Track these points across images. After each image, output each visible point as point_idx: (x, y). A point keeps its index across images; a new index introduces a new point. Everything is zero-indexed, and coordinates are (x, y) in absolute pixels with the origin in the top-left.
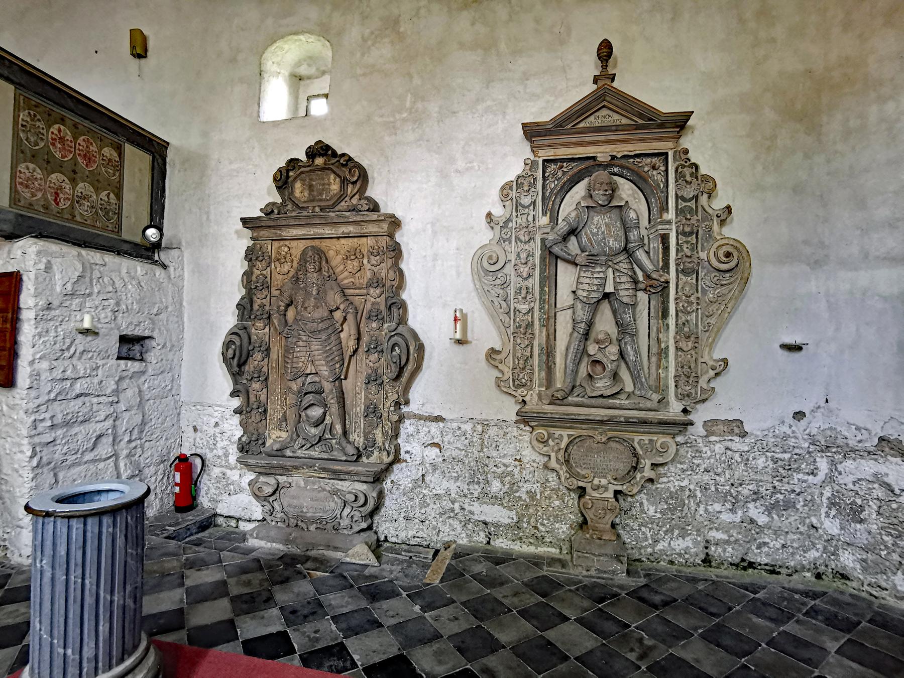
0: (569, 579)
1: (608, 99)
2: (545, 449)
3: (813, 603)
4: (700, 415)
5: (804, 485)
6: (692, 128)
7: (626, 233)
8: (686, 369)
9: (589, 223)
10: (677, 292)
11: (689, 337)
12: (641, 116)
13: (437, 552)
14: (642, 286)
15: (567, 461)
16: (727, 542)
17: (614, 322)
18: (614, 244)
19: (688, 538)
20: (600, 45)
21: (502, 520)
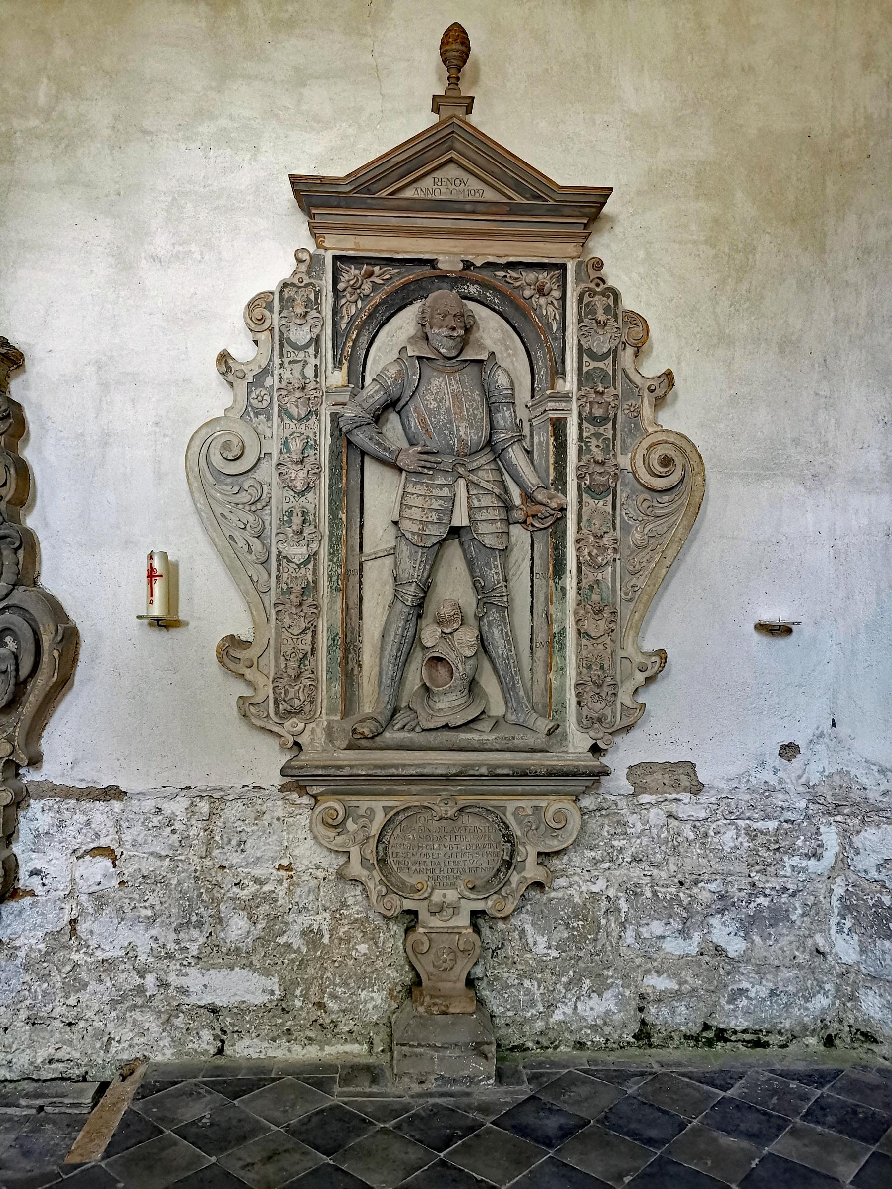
0: (384, 1107)
1: (458, 145)
2: (340, 839)
3: (819, 1092)
4: (623, 757)
5: (802, 876)
6: (611, 220)
8: (595, 671)
9: (422, 389)
10: (580, 528)
11: (600, 611)
12: (519, 188)
13: (104, 1087)
14: (518, 515)
15: (382, 861)
16: (677, 995)
17: (471, 583)
18: (469, 433)
19: (607, 995)
20: (446, 34)
21: (248, 998)
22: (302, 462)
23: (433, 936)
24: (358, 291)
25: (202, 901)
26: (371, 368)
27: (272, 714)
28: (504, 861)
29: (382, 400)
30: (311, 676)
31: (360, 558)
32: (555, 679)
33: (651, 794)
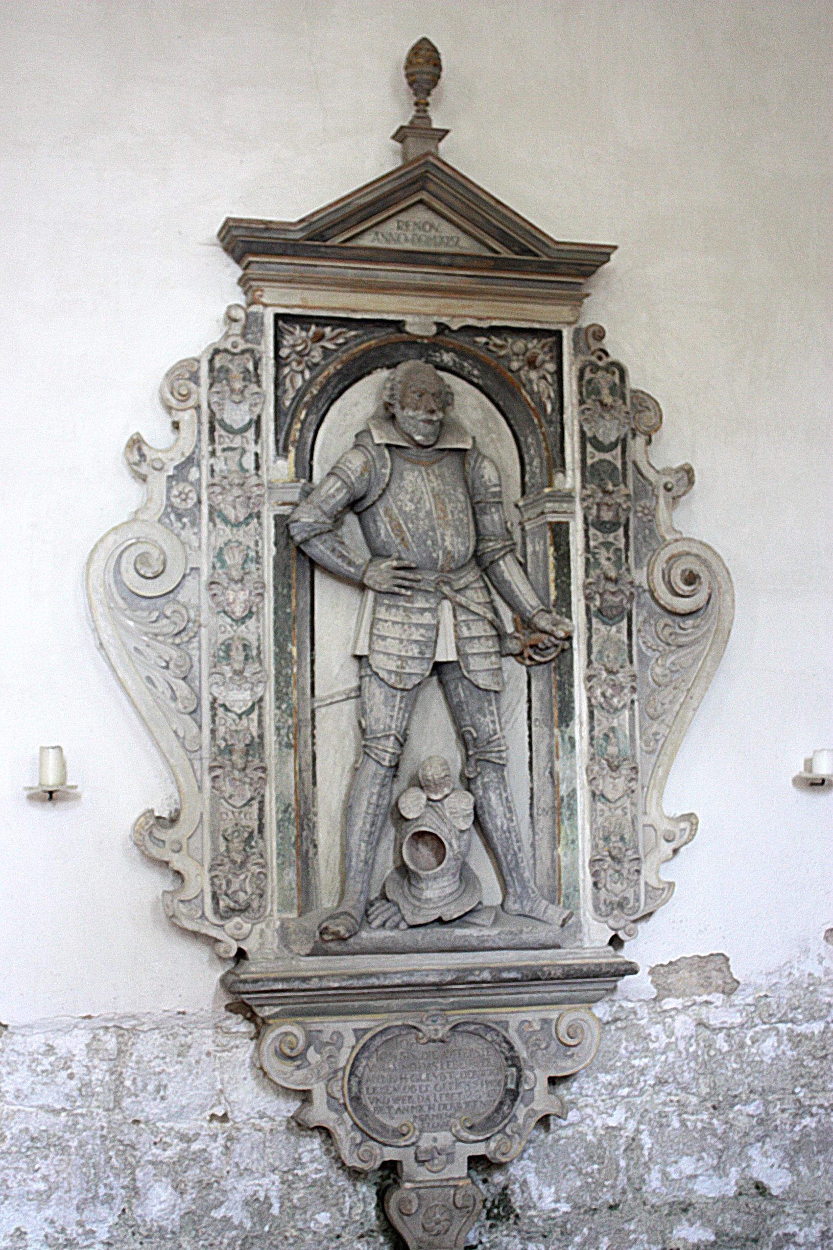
4: (647, 948)
7: (474, 514)
9: (393, 486)
10: (590, 663)
12: (505, 239)
22: (241, 580)
23: (422, 1191)
24: (306, 358)
25: (112, 1167)
26: (320, 455)
27: (209, 912)
28: (508, 1091)
29: (345, 501)
30: (261, 861)
31: (312, 704)
32: (565, 855)
33: (678, 997)
